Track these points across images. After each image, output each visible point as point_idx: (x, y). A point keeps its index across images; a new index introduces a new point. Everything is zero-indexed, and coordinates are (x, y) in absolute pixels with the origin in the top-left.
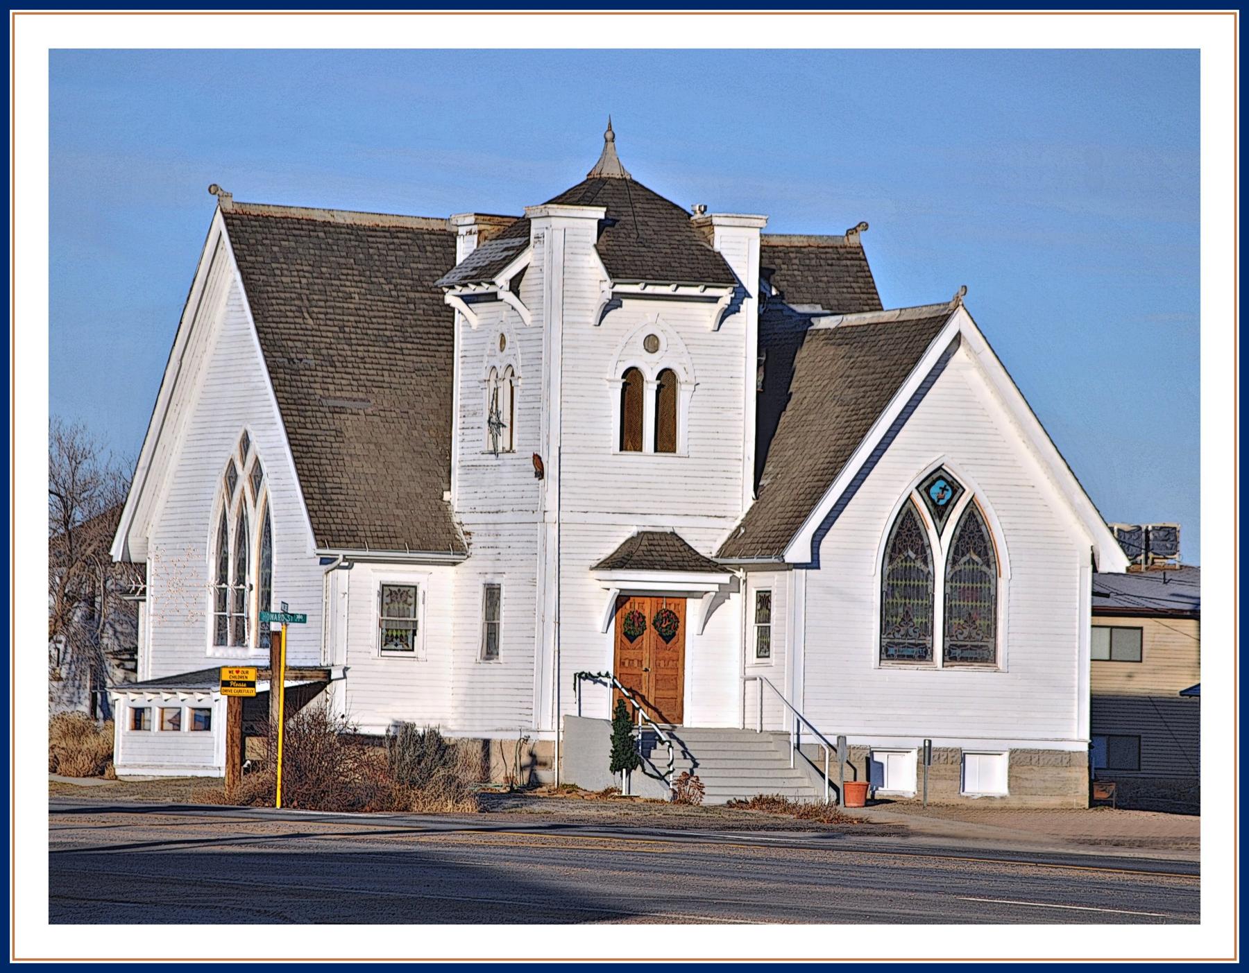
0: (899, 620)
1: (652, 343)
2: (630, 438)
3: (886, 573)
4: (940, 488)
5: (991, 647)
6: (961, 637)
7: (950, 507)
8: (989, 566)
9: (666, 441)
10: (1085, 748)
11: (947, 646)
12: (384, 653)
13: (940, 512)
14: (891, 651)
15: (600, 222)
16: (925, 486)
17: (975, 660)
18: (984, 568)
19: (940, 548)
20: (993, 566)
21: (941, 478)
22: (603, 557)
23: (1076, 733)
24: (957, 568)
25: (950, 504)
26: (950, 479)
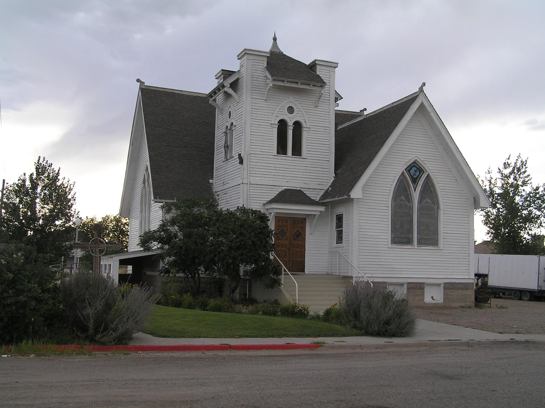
1: (291, 110)
2: (282, 149)
4: (415, 170)
7: (418, 179)
9: (297, 151)
13: (415, 181)
16: (409, 169)
21: (414, 166)
25: (419, 177)
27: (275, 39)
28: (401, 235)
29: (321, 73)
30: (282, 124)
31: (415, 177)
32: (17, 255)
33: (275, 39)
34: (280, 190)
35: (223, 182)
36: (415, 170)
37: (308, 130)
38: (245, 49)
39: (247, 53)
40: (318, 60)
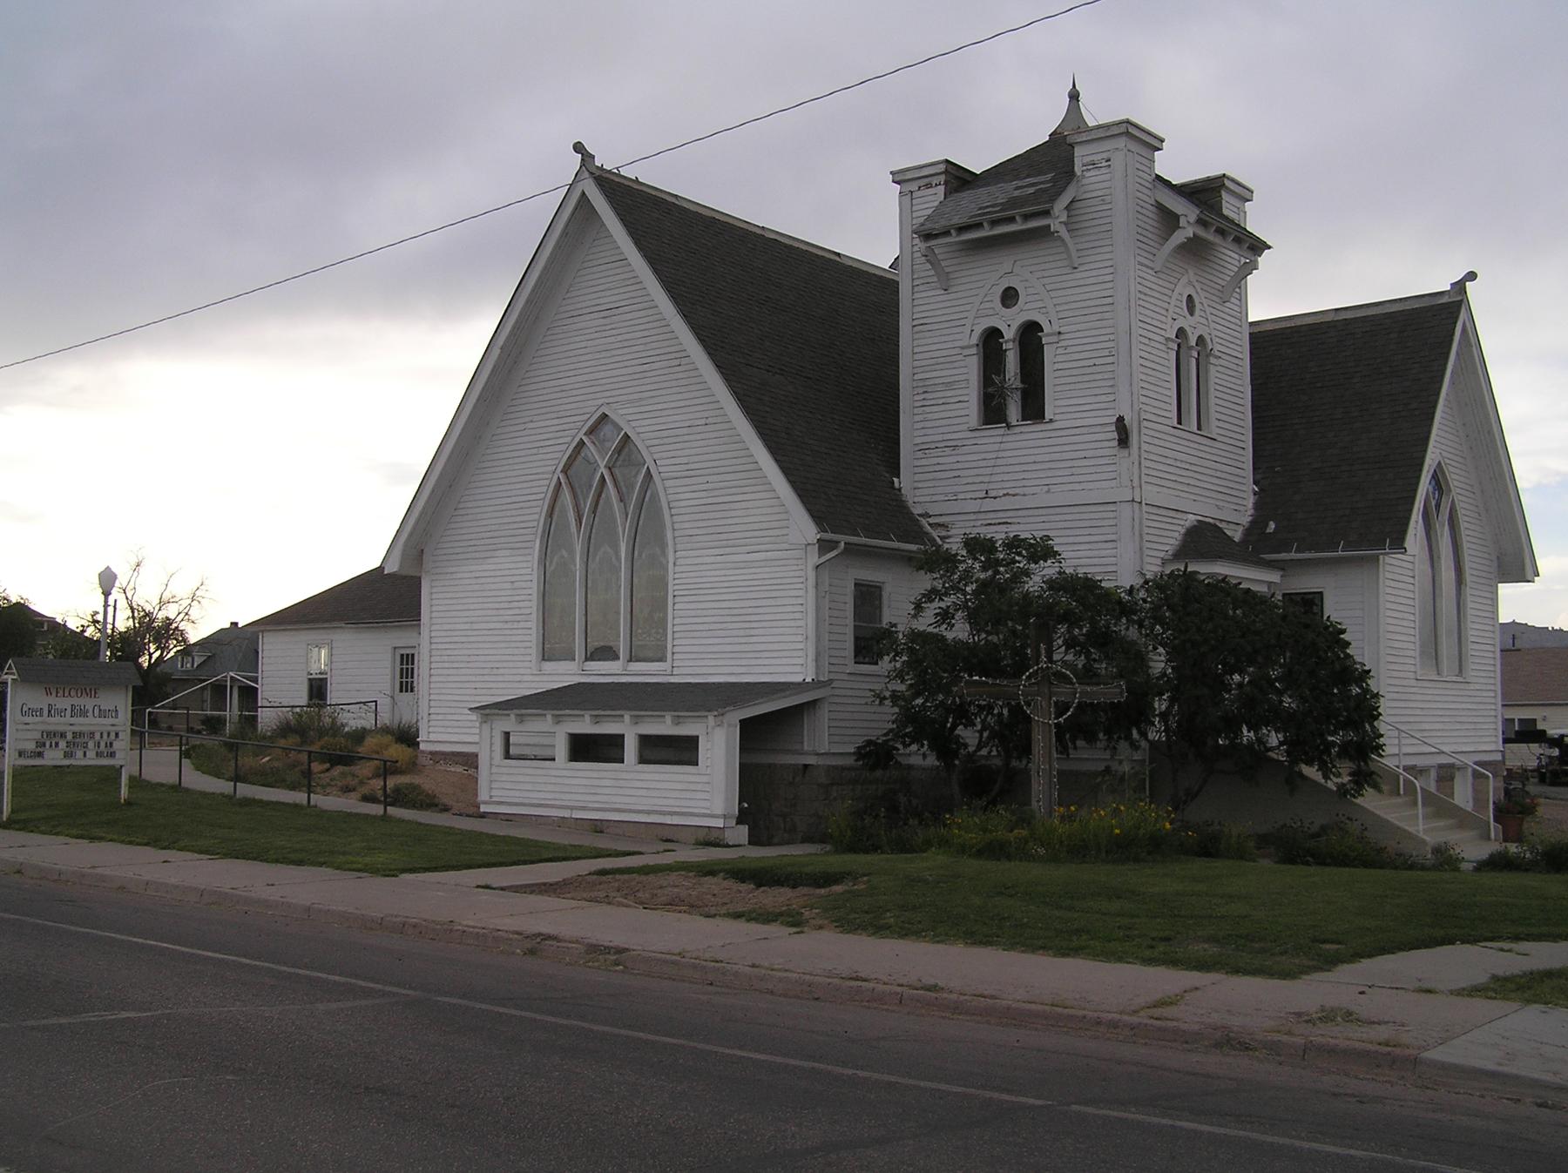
27: (1074, 96)
32: (1235, 609)
33: (1074, 96)
34: (1188, 524)
35: (984, 487)
38: (1128, 122)
39: (1127, 133)
40: (1233, 181)
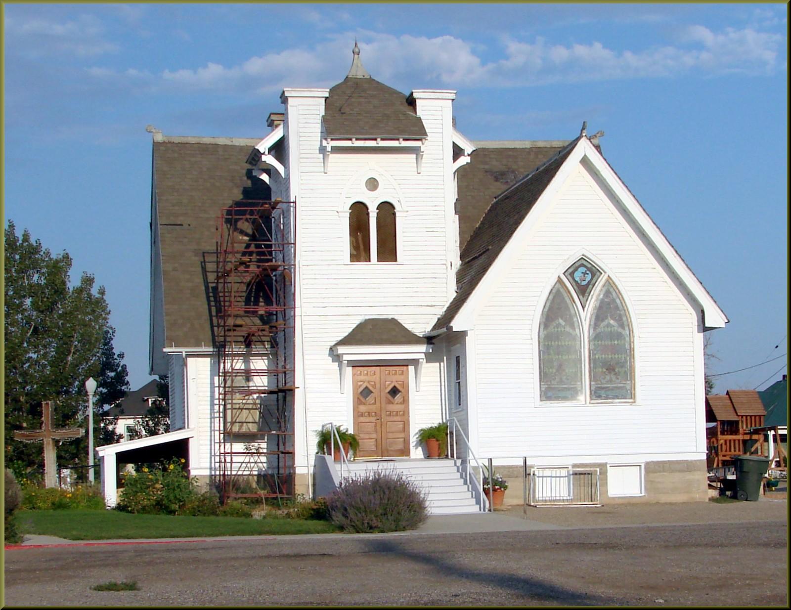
0: (554, 371)
1: (372, 184)
2: (359, 252)
3: (542, 336)
4: (584, 274)
5: (628, 387)
6: (603, 381)
7: (591, 286)
8: (623, 328)
9: (388, 252)
10: (704, 457)
11: (593, 388)
12: (593, 401)
13: (583, 290)
14: (550, 394)
15: (326, 98)
16: (570, 272)
17: (617, 397)
18: (620, 330)
19: (585, 315)
20: (627, 328)
21: (582, 265)
22: (340, 338)
23: (695, 447)
24: (598, 330)
25: (591, 284)
26: (589, 266)
28: (554, 383)
29: (424, 113)
30: (359, 211)
31: (584, 283)
36: (584, 274)
37: (405, 214)
